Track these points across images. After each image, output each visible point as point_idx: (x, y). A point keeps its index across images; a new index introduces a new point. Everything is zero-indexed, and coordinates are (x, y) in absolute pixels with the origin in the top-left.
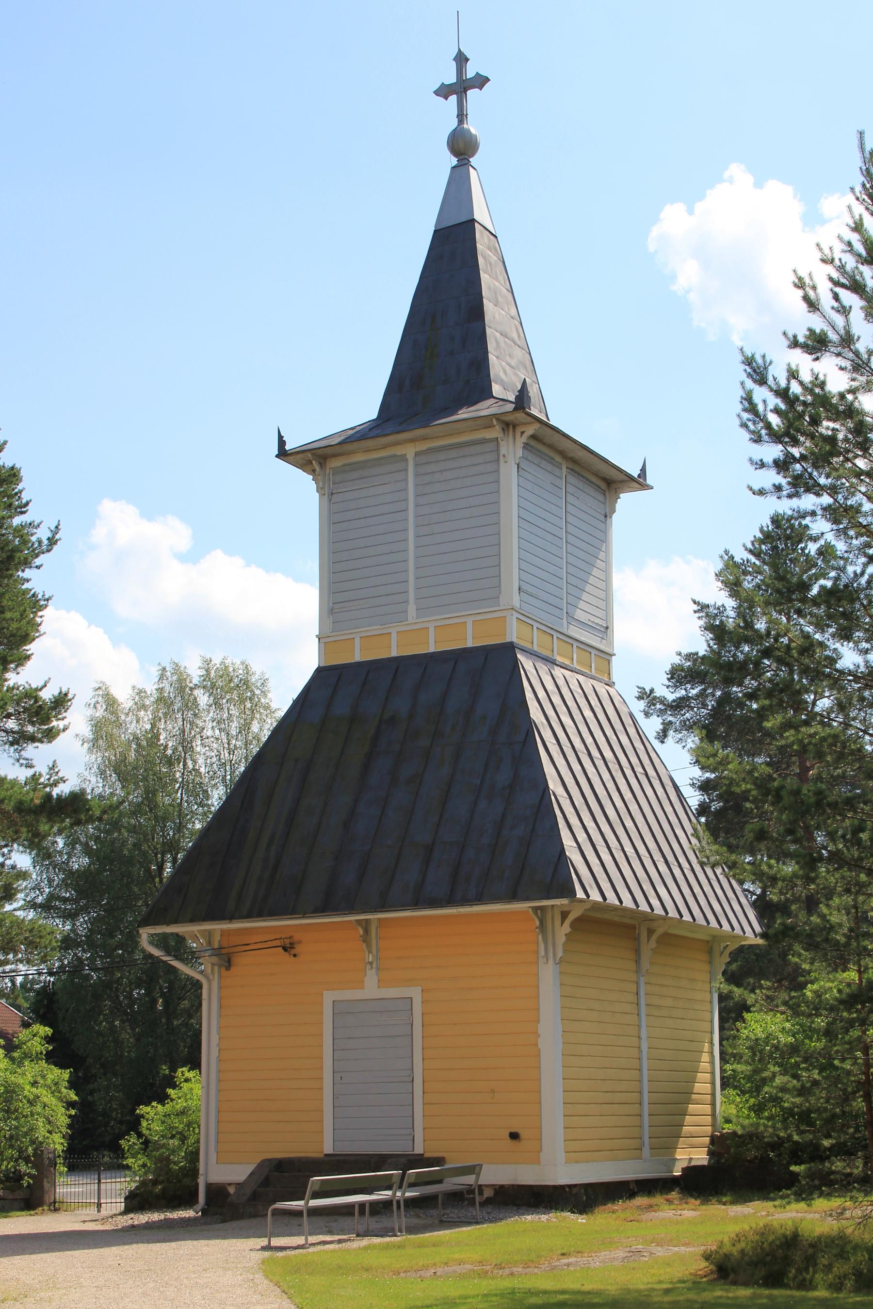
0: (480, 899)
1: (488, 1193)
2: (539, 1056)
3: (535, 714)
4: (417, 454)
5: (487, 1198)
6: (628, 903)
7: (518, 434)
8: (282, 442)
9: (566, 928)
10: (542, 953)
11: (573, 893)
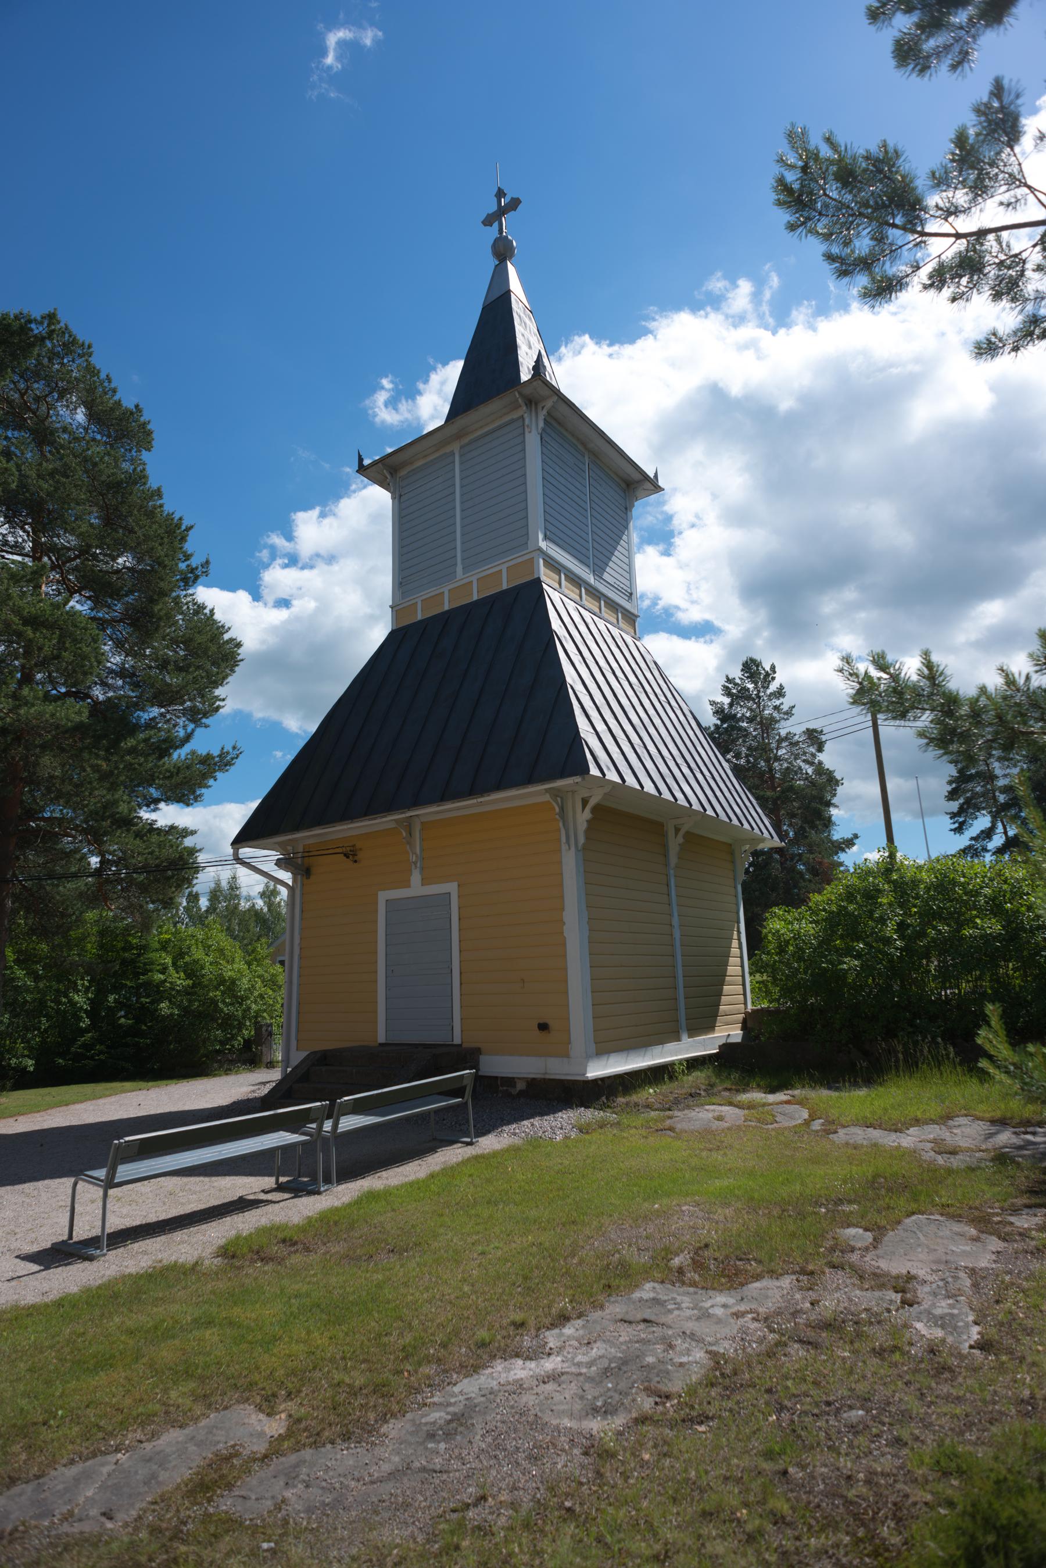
0: (499, 787)
1: (521, 1086)
2: (565, 945)
3: (556, 625)
4: (461, 447)
5: (521, 1091)
6: (649, 788)
7: (540, 408)
8: (361, 460)
9: (587, 814)
10: (564, 839)
11: (587, 770)
